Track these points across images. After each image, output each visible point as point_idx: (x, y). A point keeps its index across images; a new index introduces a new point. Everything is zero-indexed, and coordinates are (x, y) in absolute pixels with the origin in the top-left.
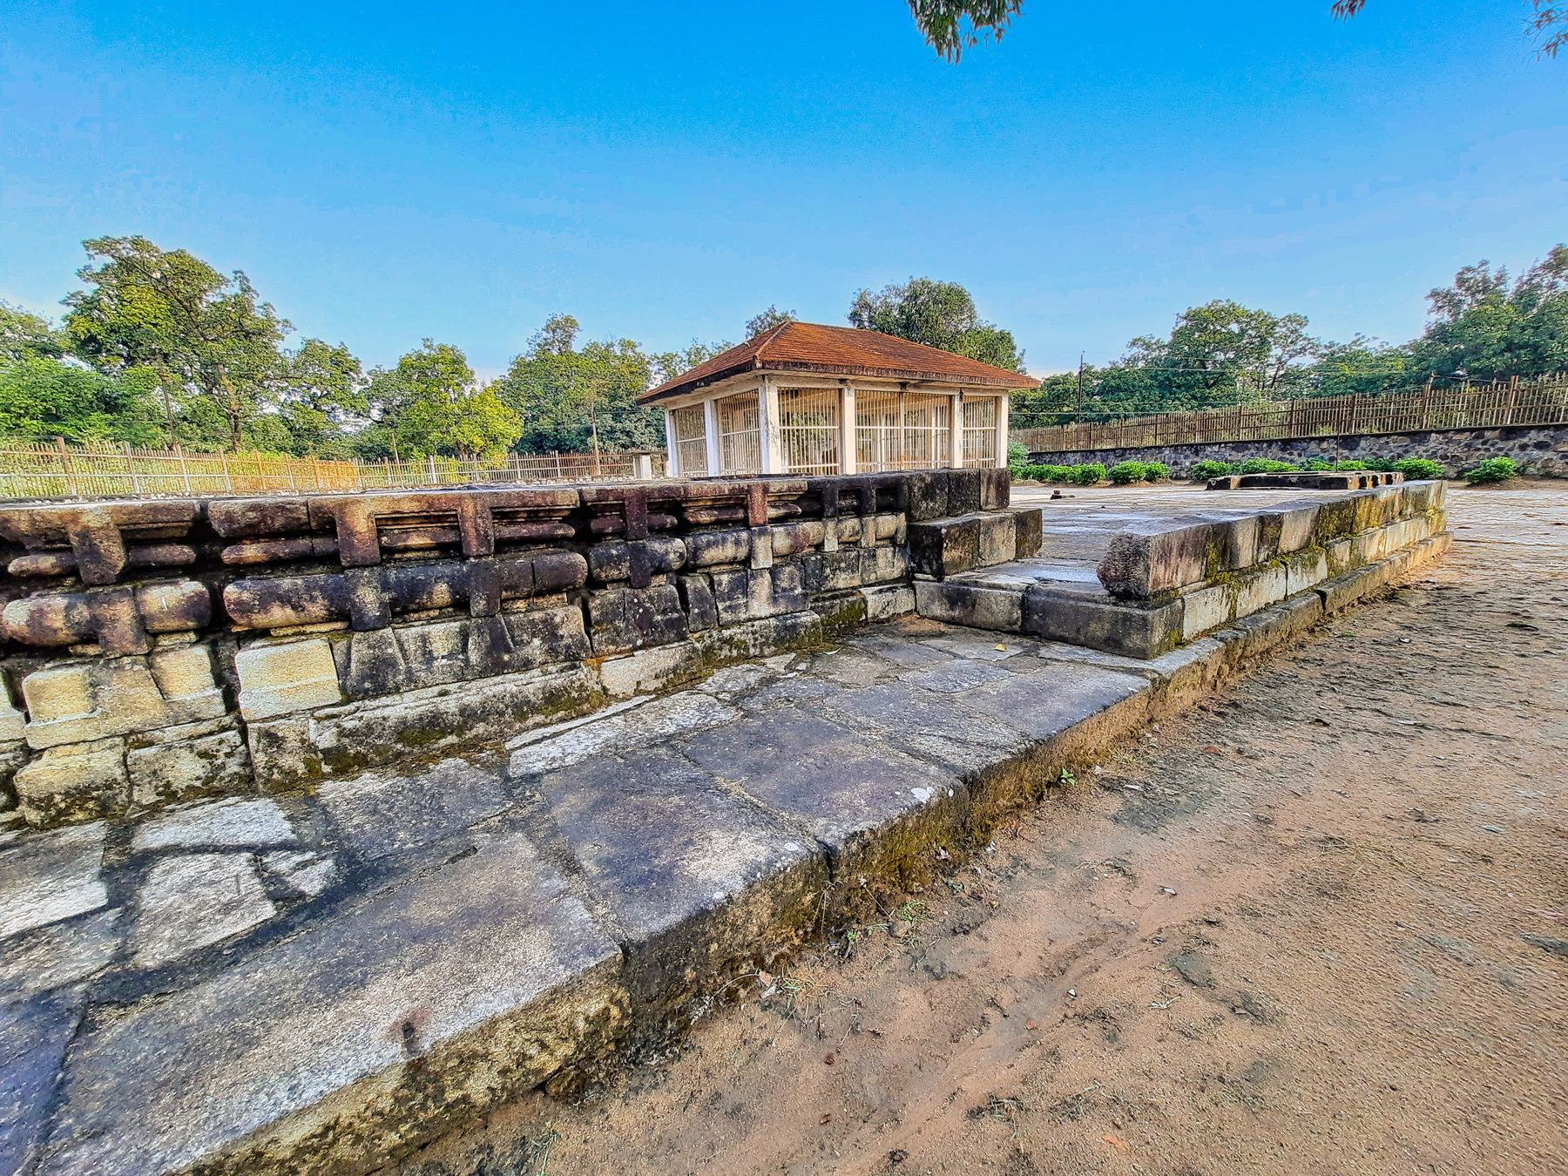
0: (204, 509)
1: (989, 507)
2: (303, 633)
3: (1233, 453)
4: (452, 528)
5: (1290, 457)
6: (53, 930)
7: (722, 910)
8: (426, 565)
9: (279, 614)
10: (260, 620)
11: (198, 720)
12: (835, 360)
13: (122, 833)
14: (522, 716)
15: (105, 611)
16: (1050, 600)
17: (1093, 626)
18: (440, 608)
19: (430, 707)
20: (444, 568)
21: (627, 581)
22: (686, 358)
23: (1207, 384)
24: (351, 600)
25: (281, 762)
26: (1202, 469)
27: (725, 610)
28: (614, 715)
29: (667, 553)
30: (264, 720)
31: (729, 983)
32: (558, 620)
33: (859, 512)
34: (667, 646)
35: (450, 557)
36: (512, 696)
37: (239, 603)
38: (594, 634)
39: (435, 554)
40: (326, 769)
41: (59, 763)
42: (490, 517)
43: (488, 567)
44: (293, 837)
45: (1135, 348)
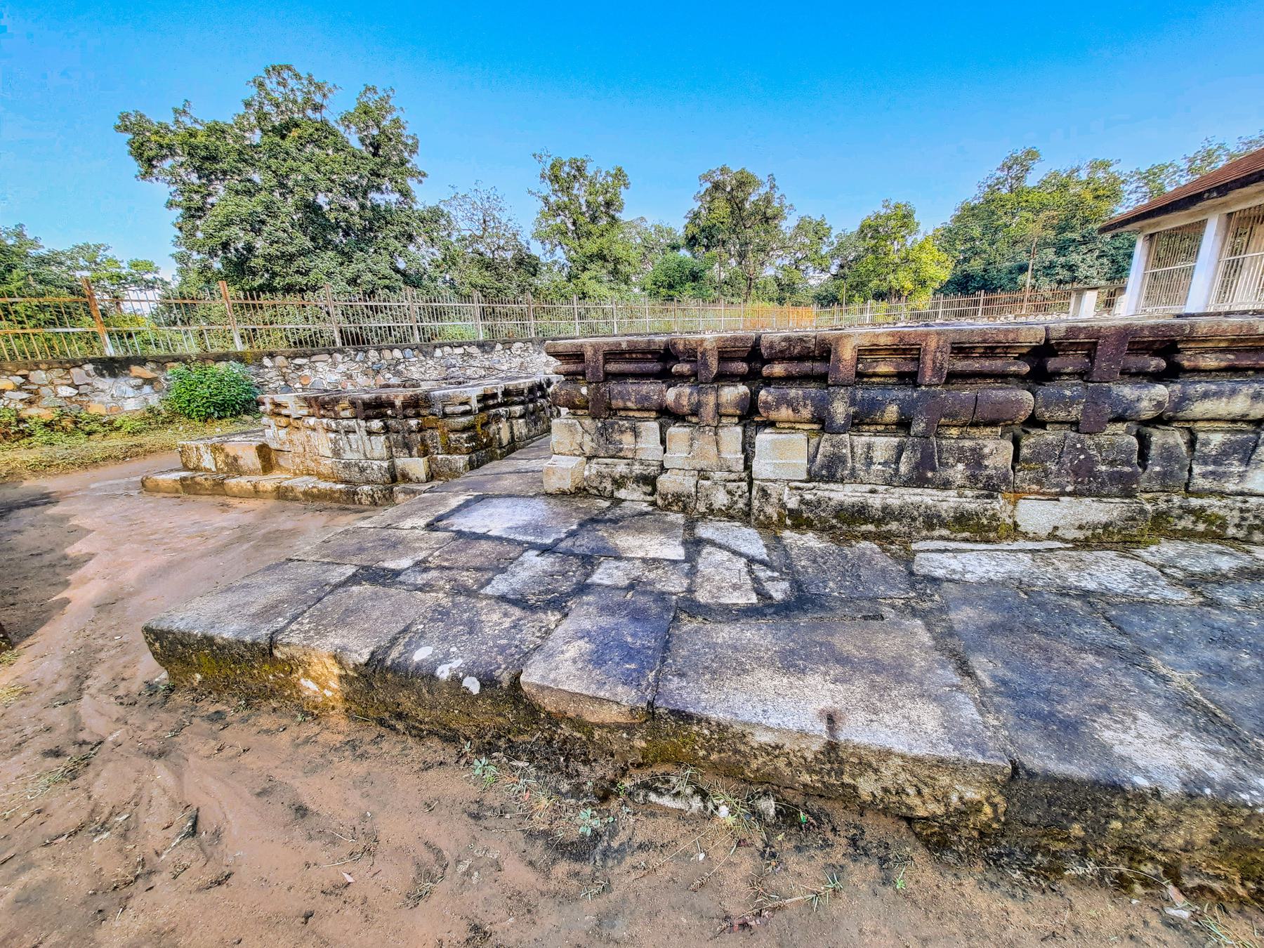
0: (758, 339)
2: (793, 428)
4: (913, 360)
6: (665, 563)
7: (1141, 798)
8: (884, 389)
9: (785, 413)
10: (773, 415)
11: (730, 471)
13: (690, 525)
14: (930, 526)
15: (703, 398)
18: (886, 425)
19: (861, 499)
20: (899, 393)
21: (1075, 425)
24: (827, 409)
25: (766, 509)
28: (1021, 551)
29: (1139, 400)
30: (762, 480)
31: (1123, 869)
32: (986, 451)
34: (1105, 500)
35: (906, 384)
36: (926, 508)
37: (766, 402)
38: (1019, 471)
39: (894, 380)
40: (788, 522)
41: (673, 477)
42: (949, 351)
43: (934, 396)
44: (767, 558)
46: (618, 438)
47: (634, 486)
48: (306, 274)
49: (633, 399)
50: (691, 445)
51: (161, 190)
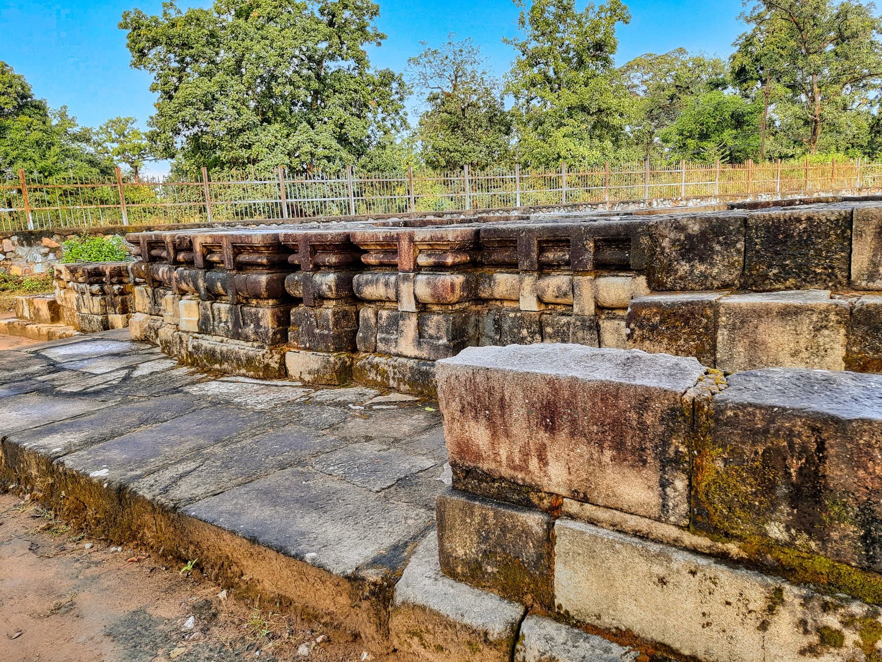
27: (381, 340)
33: (573, 267)
34: (318, 353)
48: (249, 147)
51: (147, 77)
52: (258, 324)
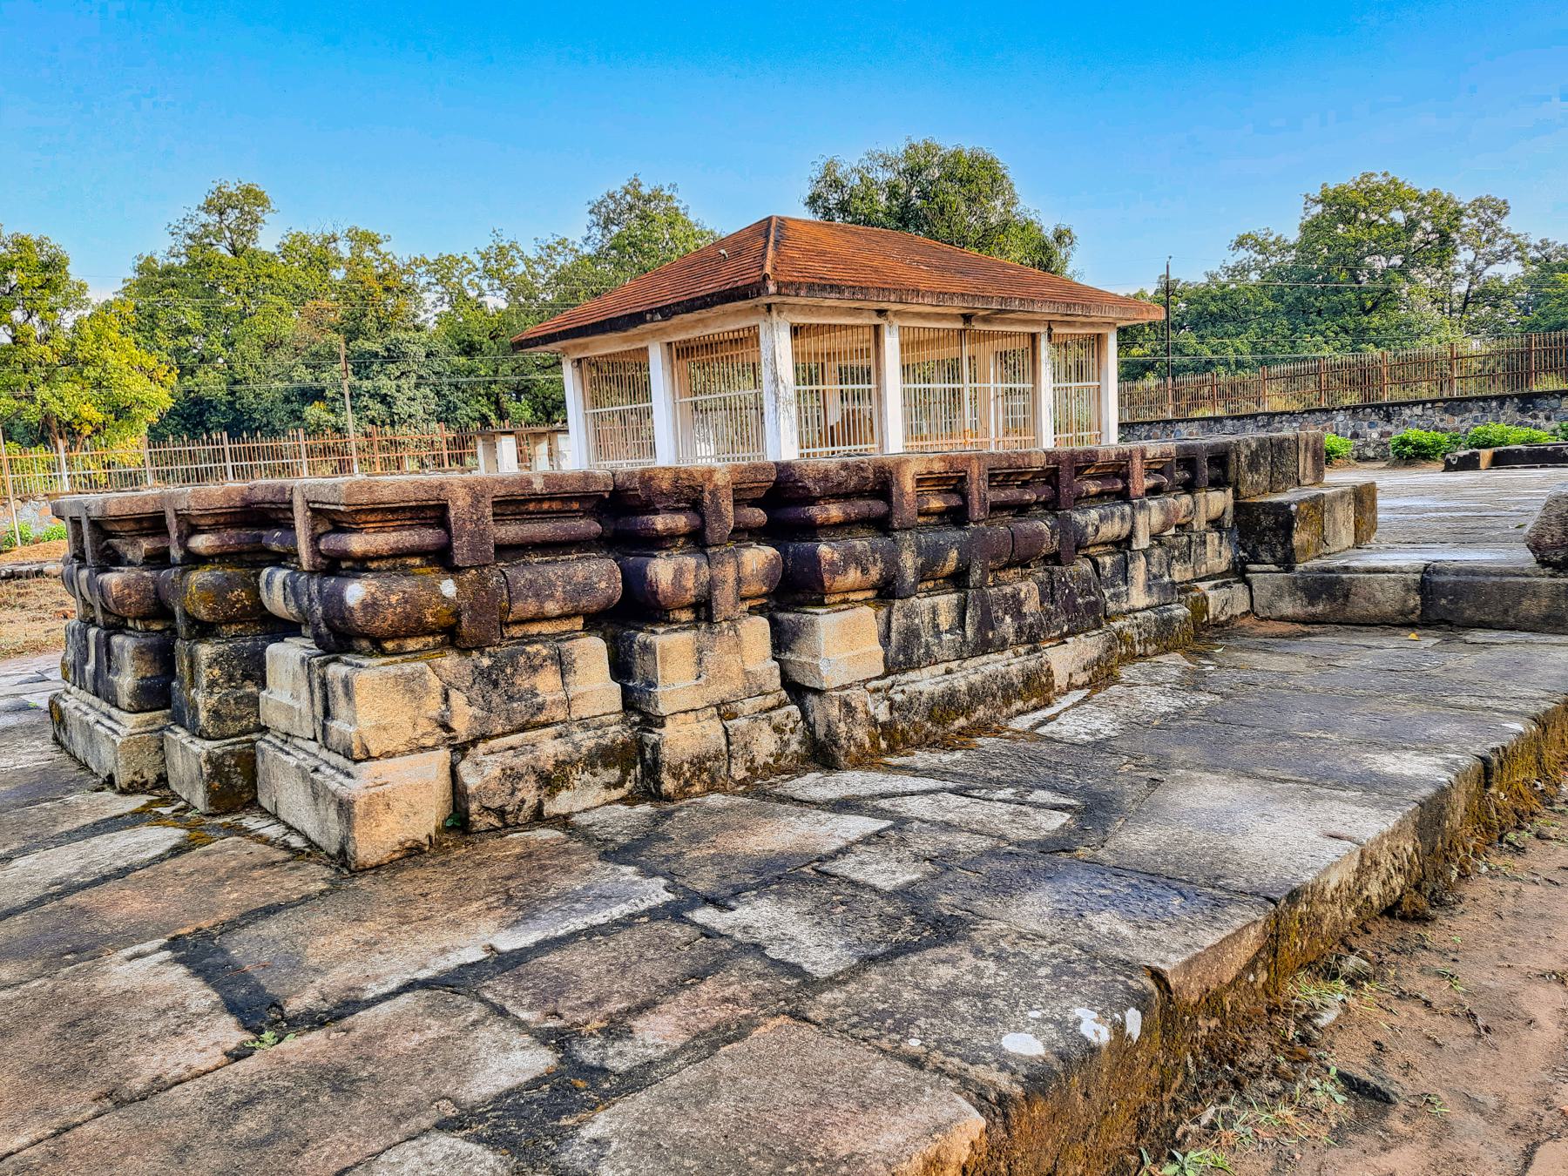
1: (1308, 481)
3: (1447, 416)
5: (1534, 422)
12: (873, 279)
16: (1463, 578)
17: (1526, 603)
22: (480, 265)
23: (1363, 308)
26: (1405, 443)
37: (832, 563)
45: (1242, 250)
46: (526, 685)
47: (587, 776)
49: (559, 594)
50: (700, 662)
52: (1019, 612)
